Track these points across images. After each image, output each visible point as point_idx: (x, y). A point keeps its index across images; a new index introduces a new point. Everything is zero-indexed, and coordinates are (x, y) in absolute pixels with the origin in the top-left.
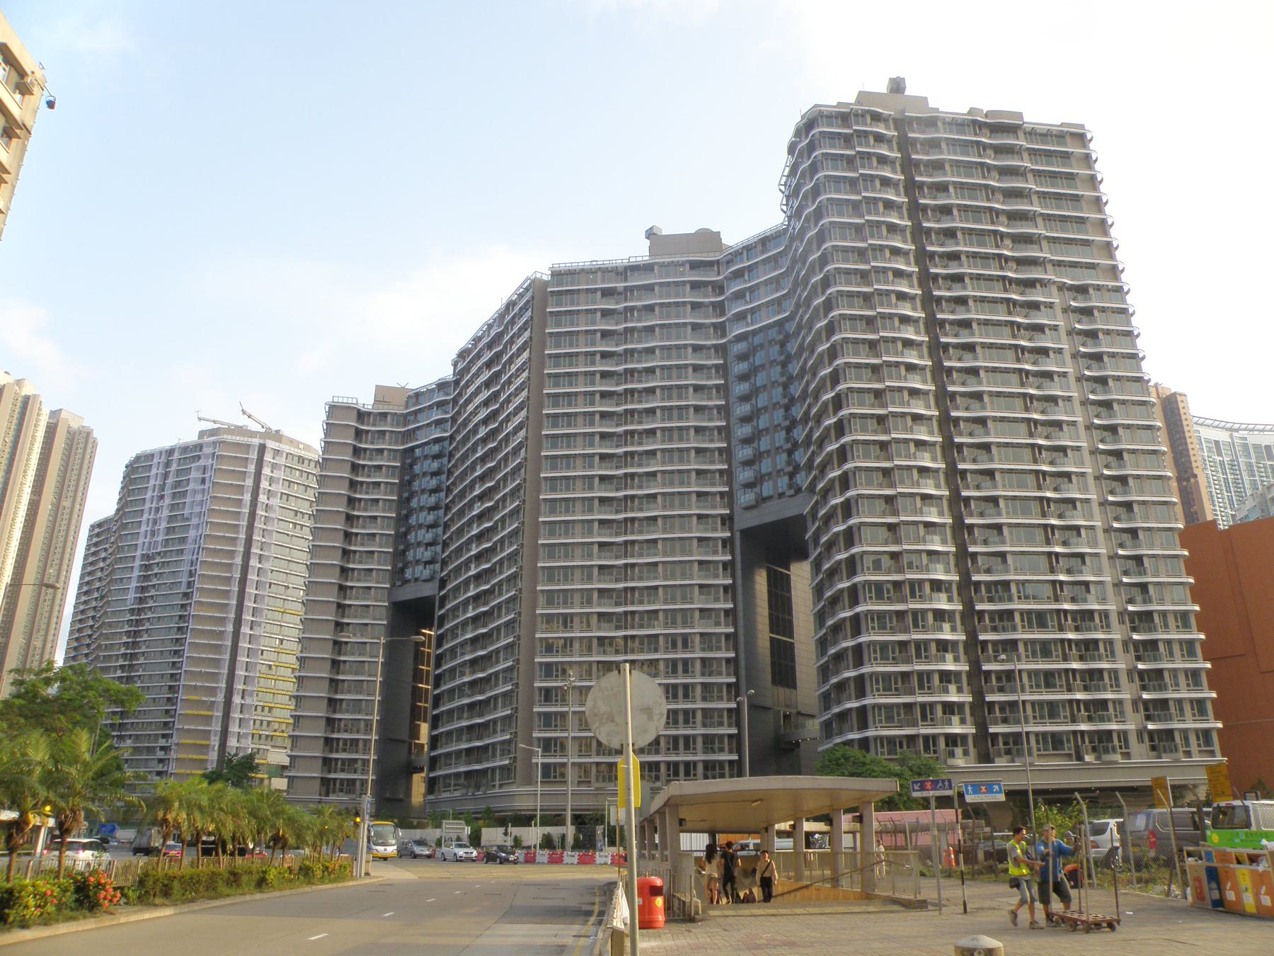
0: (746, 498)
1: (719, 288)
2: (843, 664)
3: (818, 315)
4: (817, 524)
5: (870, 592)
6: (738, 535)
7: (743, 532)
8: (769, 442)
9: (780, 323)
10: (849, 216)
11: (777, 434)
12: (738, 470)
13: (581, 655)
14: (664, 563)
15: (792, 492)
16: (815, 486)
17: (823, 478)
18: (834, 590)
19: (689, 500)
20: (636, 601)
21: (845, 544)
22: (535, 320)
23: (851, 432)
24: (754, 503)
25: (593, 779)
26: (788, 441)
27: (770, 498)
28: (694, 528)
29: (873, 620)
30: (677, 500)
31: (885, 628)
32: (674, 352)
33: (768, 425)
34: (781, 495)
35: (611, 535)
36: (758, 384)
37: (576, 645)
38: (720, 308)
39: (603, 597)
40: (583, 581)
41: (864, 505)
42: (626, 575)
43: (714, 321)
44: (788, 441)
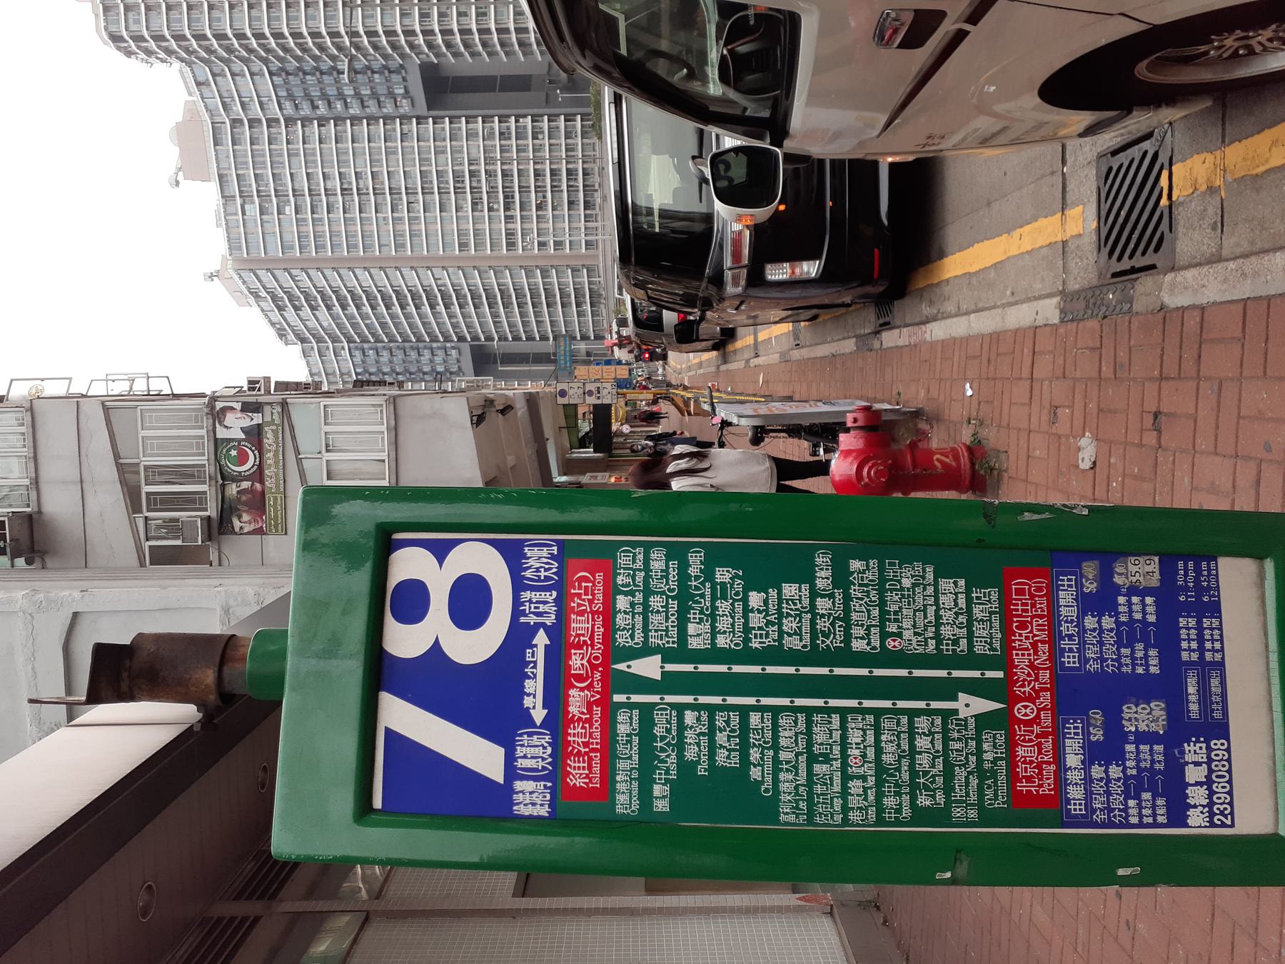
0: (405, 107)
1: (236, 122)
2: (471, 42)
3: (263, 44)
4: (288, 57)
5: (426, 21)
6: (432, 113)
7: (429, 109)
8: (331, 88)
9: (271, 74)
10: (281, 10)
11: (325, 82)
12: (302, 113)
13: (405, 224)
14: (387, 167)
15: (403, 71)
16: (262, 57)
17: (276, 51)
18: (387, 46)
19: (293, 150)
20: (431, 186)
21: (525, 33)
22: (304, 266)
23: (262, 29)
24: (309, 102)
25: (593, 212)
26: (366, 73)
27: (405, 88)
28: (411, 144)
29: (443, 21)
30: (342, 158)
31: (199, 18)
32: (310, 158)
33: (301, 89)
34: (404, 79)
35: (370, 204)
36: (319, 94)
37: (510, 226)
38: (253, 123)
39: (397, 209)
40: (355, 225)
41: (237, 25)
42: (526, 192)
43: (283, 127)
44: (366, 73)
